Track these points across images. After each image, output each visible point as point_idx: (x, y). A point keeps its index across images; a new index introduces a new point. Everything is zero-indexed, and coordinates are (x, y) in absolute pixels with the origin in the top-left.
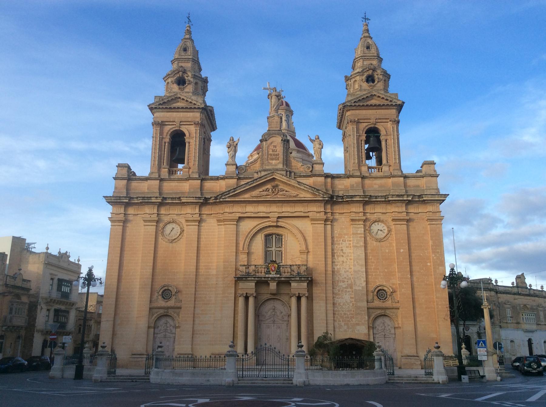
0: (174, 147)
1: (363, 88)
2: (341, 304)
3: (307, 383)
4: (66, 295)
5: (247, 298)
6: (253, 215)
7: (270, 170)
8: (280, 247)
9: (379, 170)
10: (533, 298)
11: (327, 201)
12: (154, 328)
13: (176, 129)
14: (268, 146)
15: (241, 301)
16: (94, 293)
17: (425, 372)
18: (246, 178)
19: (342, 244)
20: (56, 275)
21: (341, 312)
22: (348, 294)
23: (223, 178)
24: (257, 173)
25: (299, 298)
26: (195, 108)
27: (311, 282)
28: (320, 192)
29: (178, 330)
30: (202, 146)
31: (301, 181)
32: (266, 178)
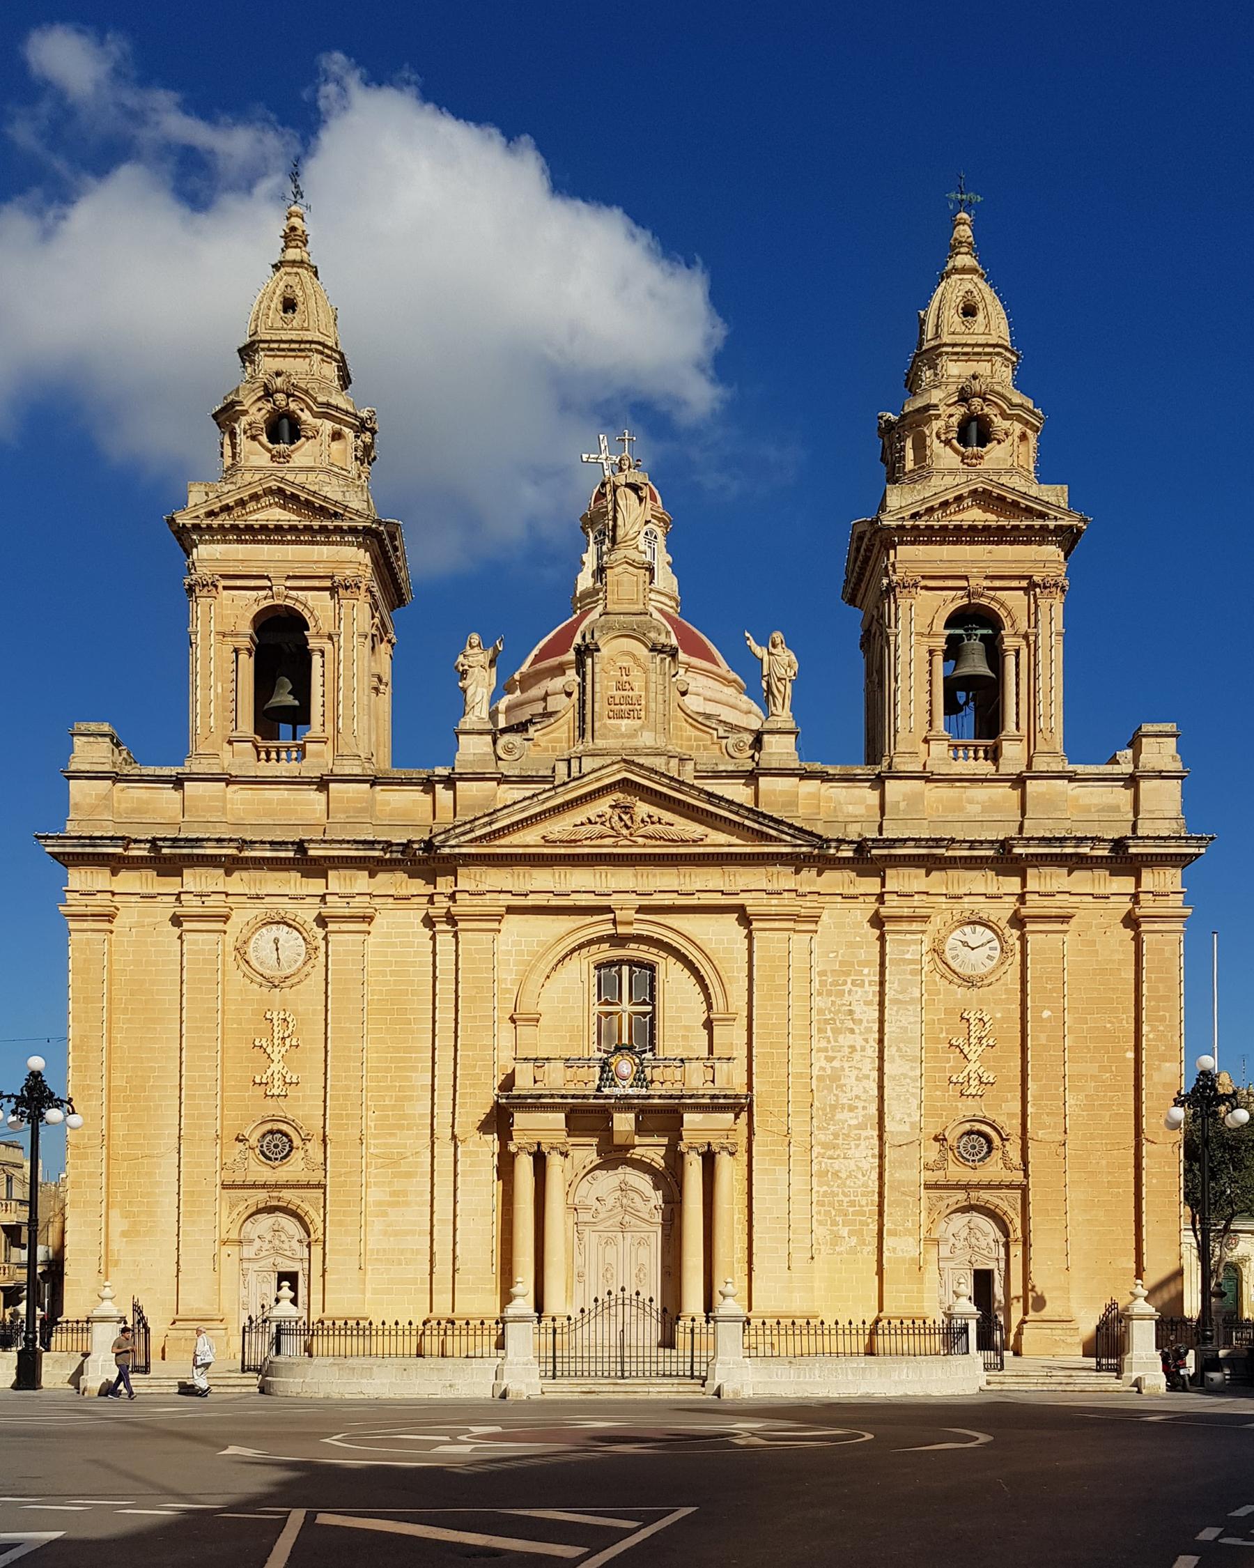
2: (843, 1175)
6: (556, 902)
19: (850, 991)
21: (841, 1197)
32: (598, 779)
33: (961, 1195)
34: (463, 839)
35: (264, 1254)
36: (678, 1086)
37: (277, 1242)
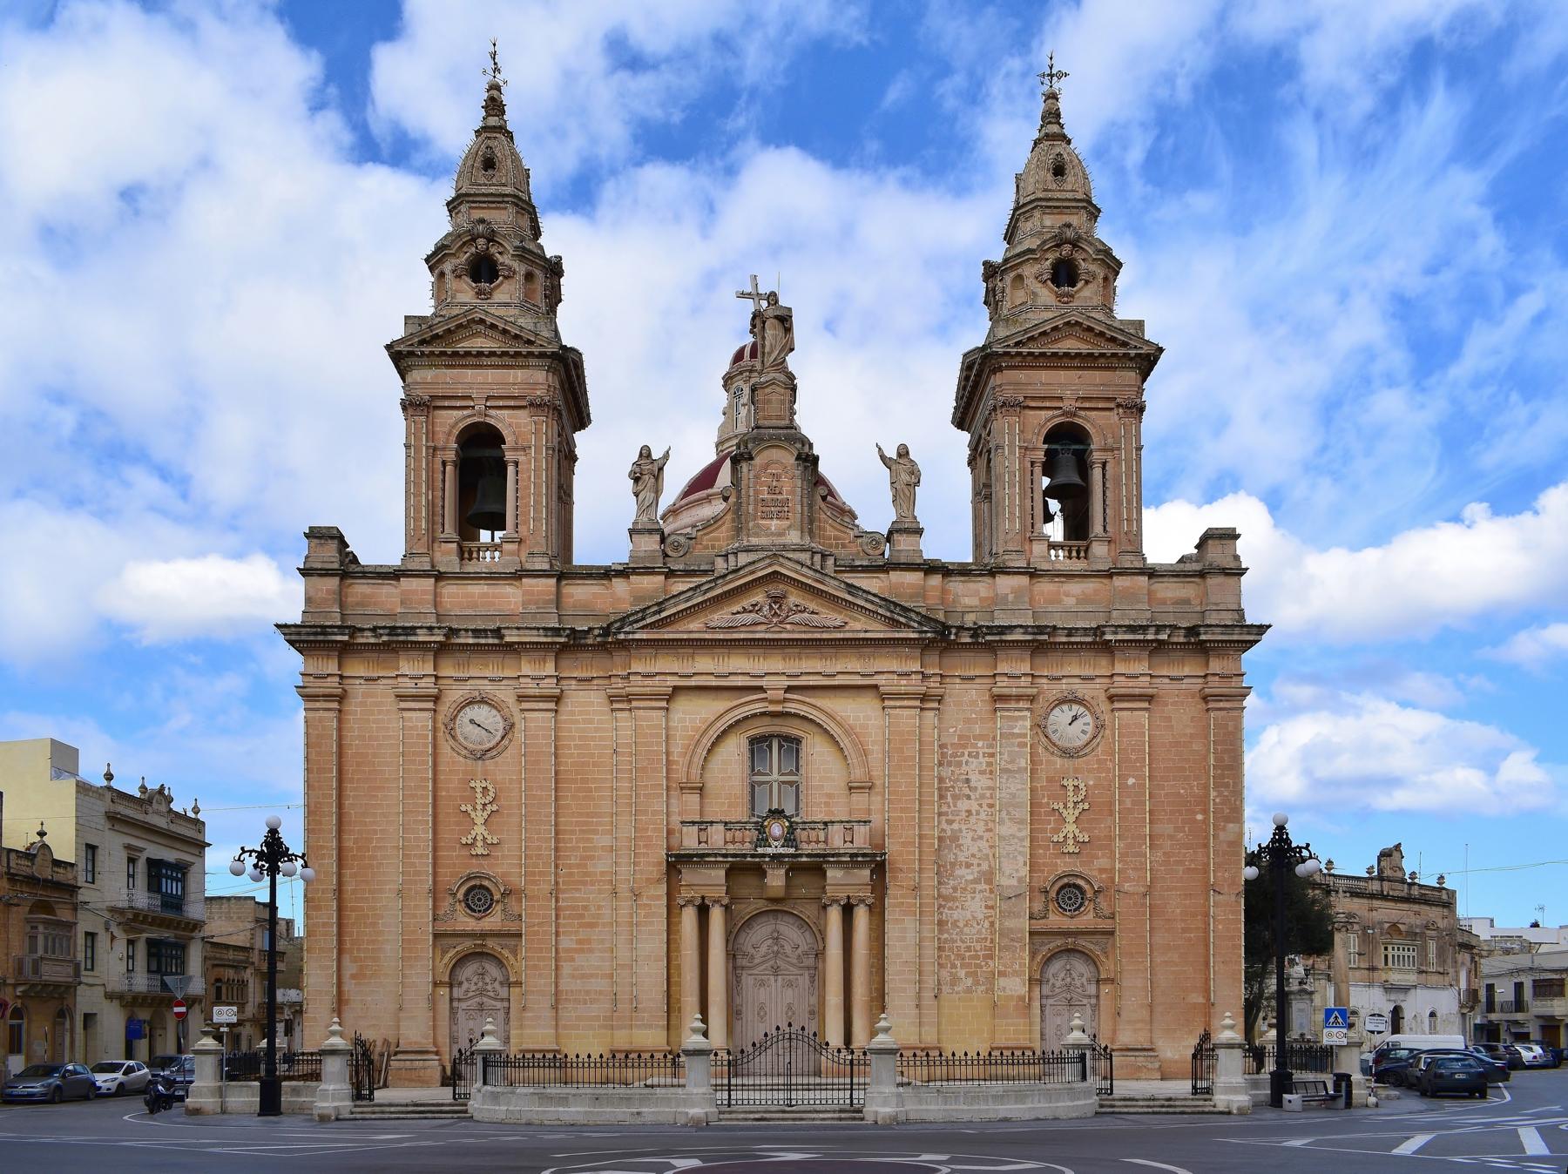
0: (472, 481)
1: (1040, 301)
2: (961, 924)
3: (902, 1118)
4: (175, 904)
5: (703, 911)
6: (714, 682)
9: (1070, 552)
10: (1416, 907)
11: (932, 641)
12: (451, 986)
13: (476, 419)
14: (757, 477)
15: (689, 918)
16: (246, 898)
17: (1194, 1087)
18: (689, 573)
20: (141, 850)
22: (978, 896)
23: (624, 573)
24: (726, 555)
25: (848, 911)
26: (530, 354)
27: (878, 866)
28: (913, 615)
29: (515, 991)
30: (555, 473)
31: (856, 583)
32: (753, 572)
33: (1059, 942)
36: (822, 846)
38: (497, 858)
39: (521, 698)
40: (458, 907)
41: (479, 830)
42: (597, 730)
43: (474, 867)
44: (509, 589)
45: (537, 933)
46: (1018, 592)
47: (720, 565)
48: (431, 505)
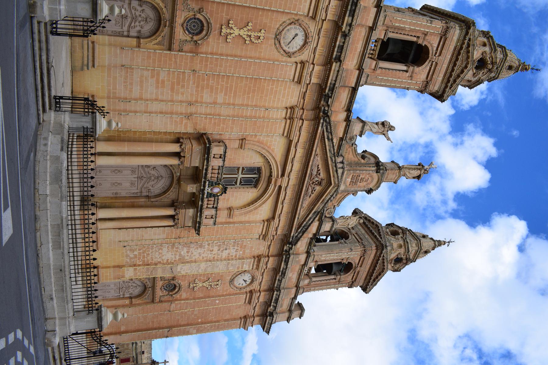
2: (160, 251)
7: (341, 178)
8: (241, 182)
13: (430, 55)
15: (175, 148)
21: (151, 251)
28: (301, 235)
32: (334, 176)
34: (325, 128)
35: (133, 11)
37: (140, 19)
38: (218, 39)
39: (302, 63)
40: (191, 13)
41: (236, 32)
42: (279, 99)
43: (215, 26)
44: (355, 62)
45: (170, 60)
46: (299, 261)
47: (339, 159)
48: (403, 29)
